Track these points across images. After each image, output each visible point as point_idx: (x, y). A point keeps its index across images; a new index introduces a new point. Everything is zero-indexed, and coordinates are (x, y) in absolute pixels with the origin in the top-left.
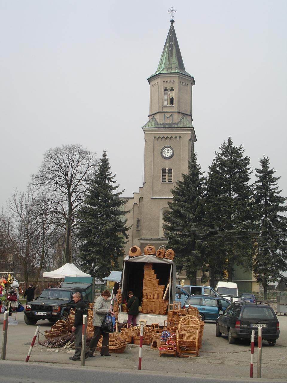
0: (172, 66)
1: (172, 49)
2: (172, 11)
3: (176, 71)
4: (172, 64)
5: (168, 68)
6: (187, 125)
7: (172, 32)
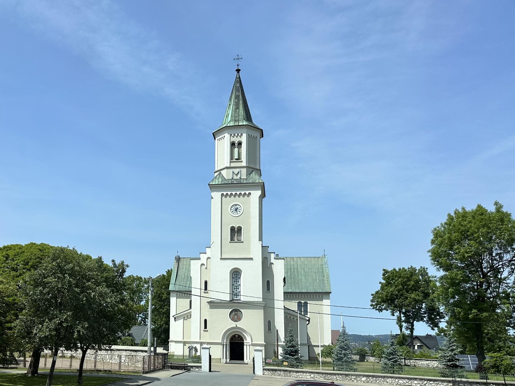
1: (239, 100)
3: (244, 124)
4: (239, 116)
5: (235, 121)
6: (257, 181)
7: (239, 81)
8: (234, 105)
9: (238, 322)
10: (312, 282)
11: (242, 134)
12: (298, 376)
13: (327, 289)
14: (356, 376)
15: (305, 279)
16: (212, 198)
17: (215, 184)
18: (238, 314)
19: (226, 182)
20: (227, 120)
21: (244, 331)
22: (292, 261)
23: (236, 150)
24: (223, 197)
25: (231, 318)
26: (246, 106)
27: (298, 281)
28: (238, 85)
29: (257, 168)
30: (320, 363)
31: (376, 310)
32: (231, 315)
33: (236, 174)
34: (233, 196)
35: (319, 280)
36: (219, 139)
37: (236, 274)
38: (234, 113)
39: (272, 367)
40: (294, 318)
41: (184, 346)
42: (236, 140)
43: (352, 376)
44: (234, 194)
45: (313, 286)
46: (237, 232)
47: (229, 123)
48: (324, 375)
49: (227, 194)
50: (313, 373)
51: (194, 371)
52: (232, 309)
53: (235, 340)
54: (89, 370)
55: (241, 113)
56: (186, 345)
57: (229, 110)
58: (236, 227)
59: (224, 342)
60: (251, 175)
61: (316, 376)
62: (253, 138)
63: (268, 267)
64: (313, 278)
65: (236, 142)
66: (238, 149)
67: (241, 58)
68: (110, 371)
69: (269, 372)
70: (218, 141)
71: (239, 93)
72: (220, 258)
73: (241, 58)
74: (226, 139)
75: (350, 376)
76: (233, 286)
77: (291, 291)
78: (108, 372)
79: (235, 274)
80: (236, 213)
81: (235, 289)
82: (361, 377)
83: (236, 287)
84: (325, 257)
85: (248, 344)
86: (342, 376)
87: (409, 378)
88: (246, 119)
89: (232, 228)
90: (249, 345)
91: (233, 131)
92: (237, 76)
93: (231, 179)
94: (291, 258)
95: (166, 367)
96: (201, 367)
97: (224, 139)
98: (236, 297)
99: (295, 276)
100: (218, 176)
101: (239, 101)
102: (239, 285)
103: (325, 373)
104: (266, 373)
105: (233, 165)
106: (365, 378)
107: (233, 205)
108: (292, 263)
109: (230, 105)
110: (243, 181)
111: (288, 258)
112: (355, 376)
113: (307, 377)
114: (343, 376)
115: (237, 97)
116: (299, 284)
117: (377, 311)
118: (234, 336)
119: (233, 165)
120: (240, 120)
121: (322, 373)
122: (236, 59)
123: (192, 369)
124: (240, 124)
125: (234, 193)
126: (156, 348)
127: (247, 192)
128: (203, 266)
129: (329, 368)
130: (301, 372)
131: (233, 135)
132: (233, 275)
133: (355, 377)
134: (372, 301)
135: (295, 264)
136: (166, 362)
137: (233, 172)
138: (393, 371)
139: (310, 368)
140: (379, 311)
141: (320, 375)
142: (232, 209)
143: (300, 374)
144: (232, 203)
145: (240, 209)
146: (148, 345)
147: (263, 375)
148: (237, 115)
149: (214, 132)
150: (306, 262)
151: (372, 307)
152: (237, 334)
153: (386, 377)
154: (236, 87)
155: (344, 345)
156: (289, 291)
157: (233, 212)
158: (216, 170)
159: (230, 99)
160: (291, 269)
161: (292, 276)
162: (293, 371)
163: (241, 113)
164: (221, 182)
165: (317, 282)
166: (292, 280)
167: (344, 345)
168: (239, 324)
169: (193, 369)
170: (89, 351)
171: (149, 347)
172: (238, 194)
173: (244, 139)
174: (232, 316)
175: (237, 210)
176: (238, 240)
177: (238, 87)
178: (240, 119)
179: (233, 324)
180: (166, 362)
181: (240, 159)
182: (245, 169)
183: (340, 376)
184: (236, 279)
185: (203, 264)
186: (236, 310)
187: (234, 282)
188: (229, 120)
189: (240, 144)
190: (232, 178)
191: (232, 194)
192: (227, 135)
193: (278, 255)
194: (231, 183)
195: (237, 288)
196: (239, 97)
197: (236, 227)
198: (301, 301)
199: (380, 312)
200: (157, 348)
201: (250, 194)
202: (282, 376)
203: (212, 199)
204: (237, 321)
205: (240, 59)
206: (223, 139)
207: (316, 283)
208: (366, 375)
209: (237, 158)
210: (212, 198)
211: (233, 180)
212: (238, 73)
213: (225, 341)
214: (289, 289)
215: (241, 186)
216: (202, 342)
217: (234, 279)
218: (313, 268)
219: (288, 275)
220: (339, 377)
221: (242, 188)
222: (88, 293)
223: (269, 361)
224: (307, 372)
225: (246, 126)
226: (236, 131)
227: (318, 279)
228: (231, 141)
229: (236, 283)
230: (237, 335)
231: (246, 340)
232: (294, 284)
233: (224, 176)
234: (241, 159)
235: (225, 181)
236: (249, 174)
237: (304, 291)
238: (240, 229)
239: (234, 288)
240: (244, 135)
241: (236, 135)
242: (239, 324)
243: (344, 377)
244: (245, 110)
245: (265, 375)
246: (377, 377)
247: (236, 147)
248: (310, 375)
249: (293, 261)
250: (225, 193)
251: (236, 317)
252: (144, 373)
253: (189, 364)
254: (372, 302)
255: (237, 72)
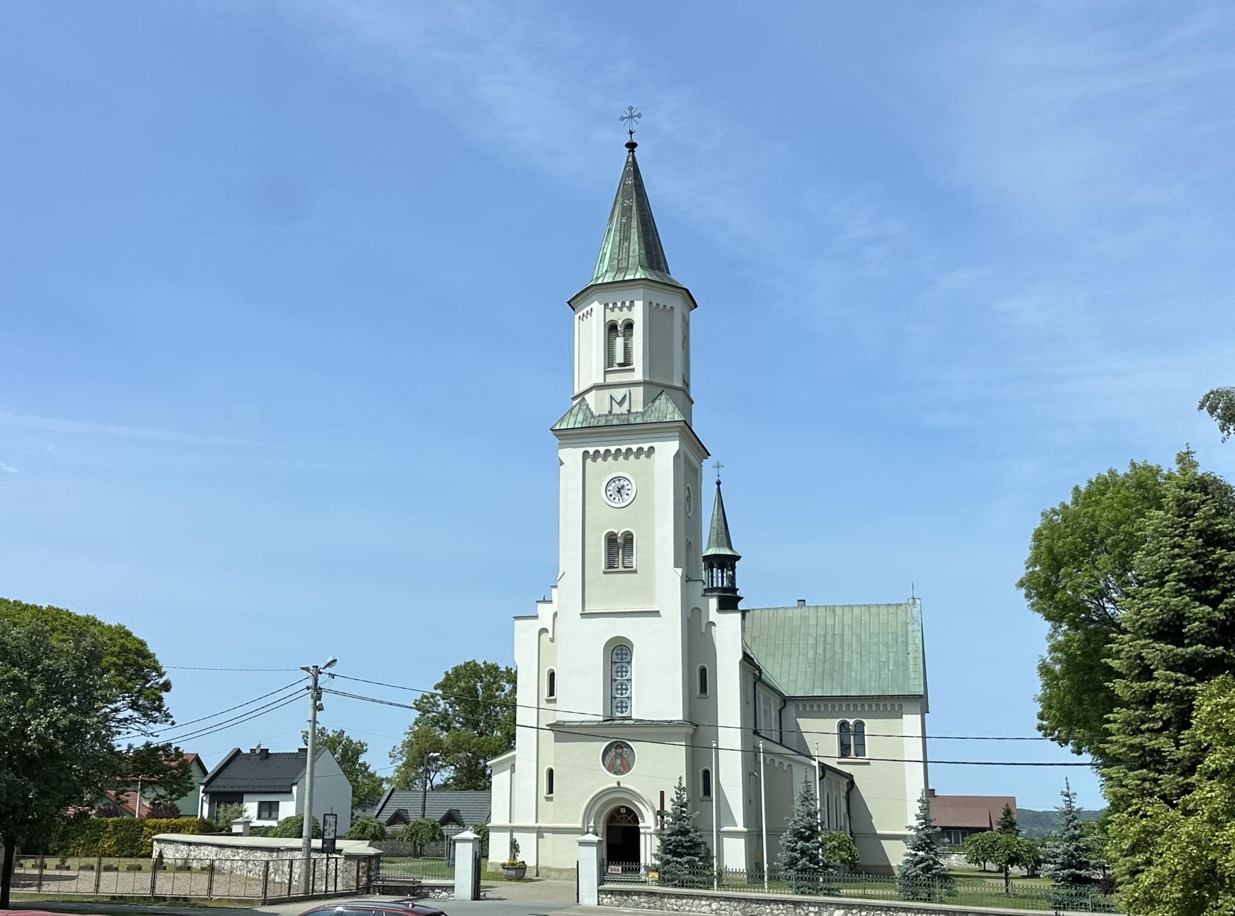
0: (630, 262)
1: (630, 218)
2: (631, 117)
3: (638, 276)
4: (629, 257)
5: (619, 270)
6: (668, 416)
7: (634, 170)
8: (619, 233)
9: (617, 775)
10: (878, 669)
11: (632, 302)
12: (680, 907)
13: (912, 687)
14: (819, 907)
15: (861, 661)
16: (562, 464)
17: (565, 428)
18: (623, 754)
19: (594, 422)
20: (601, 269)
21: (639, 797)
22: (830, 616)
23: (619, 342)
24: (589, 461)
25: (607, 765)
26: (648, 231)
27: (842, 666)
28: (631, 180)
29: (676, 384)
30: (764, 875)
31: (1052, 740)
32: (607, 757)
33: (618, 402)
34: (611, 457)
35: (896, 664)
36: (581, 317)
37: (622, 652)
38: (616, 250)
39: (436, 880)
40: (791, 766)
41: (540, 839)
42: (619, 317)
43: (808, 906)
44: (613, 452)
45: (877, 679)
46: (622, 545)
47: (601, 276)
48: (742, 905)
49: (597, 452)
50: (716, 899)
51: (436, 897)
52: (609, 742)
53: (620, 822)
54: (137, 897)
55: (634, 251)
56: (543, 837)
57: (607, 243)
58: (619, 535)
59: (588, 827)
60: (657, 402)
61: (723, 908)
62: (662, 310)
63: (703, 634)
64: (881, 660)
65: (620, 322)
66: (625, 340)
67: (639, 116)
68: (185, 899)
69: (613, 899)
70: (581, 320)
71: (632, 202)
72: (581, 614)
73: (639, 116)
74: (593, 319)
75: (804, 905)
76: (614, 684)
77: (821, 695)
78: (181, 901)
79: (619, 652)
80: (619, 500)
81: (619, 691)
82: (832, 909)
83: (622, 687)
84: (914, 603)
85: (648, 831)
86: (785, 907)
87: (949, 911)
88: (646, 265)
89: (611, 535)
90: (651, 834)
91: (610, 296)
92: (627, 159)
93: (606, 415)
94: (828, 609)
95: (372, 890)
96: (452, 887)
97: (590, 314)
98: (622, 712)
99: (834, 653)
100: (578, 407)
101: (631, 221)
102: (628, 680)
103: (746, 900)
104: (605, 901)
105: (612, 379)
106: (842, 911)
107: (613, 480)
108: (830, 621)
109: (609, 230)
110: (635, 419)
111: (819, 609)
112: (818, 906)
113: (703, 909)
114: (788, 906)
115: (626, 211)
116: (842, 675)
117: (1056, 743)
118: (617, 811)
119: (612, 379)
120: (631, 269)
121: (738, 898)
122: (626, 118)
123: (432, 895)
124: (627, 278)
125: (613, 449)
126: (335, 842)
127: (646, 447)
128: (544, 635)
129: (852, 891)
130: (688, 898)
131: (611, 305)
132: (614, 656)
133: (817, 909)
134: (1041, 717)
135: (836, 624)
136: (371, 876)
137: (611, 396)
138: (929, 896)
139: (786, 892)
140: (1060, 744)
141: (732, 904)
142: (610, 488)
143: (684, 901)
144: (610, 474)
145: (628, 487)
146: (304, 835)
147: (598, 905)
148: (624, 255)
149: (571, 300)
150: (865, 618)
151: (1040, 734)
152: (623, 807)
153: (893, 909)
154: (625, 187)
155: (805, 827)
156: (815, 695)
157: (611, 495)
158: (576, 392)
159: (611, 218)
160: (825, 636)
161: (828, 656)
162: (670, 895)
163: (634, 251)
164: (582, 423)
165: (890, 668)
166: (827, 665)
167: (805, 827)
168: (627, 780)
169: (434, 892)
170: (242, 852)
171: (306, 839)
172: (624, 451)
173: (637, 314)
174: (607, 762)
175: (622, 491)
176: (625, 567)
177: (629, 186)
178: (632, 264)
179: (611, 780)
180: (371, 876)
181: (629, 365)
182: (641, 389)
183: (781, 905)
184: (621, 664)
185: (543, 630)
186: (619, 743)
187: (617, 672)
188: (605, 269)
189: (629, 326)
190: (610, 412)
191: (608, 451)
192: (597, 307)
193: (804, 601)
194: (604, 424)
195: (624, 687)
196: (631, 211)
197: (619, 535)
198: (848, 720)
199: (1062, 746)
200: (337, 841)
201: (652, 449)
202: (643, 907)
203: (561, 465)
204: (622, 773)
205: (635, 116)
206: (589, 315)
207: (886, 671)
208: (845, 904)
209: (622, 361)
210: (562, 464)
211: (610, 417)
212: (631, 153)
213: (592, 824)
214: (815, 690)
215: (609, 432)
216: (540, 827)
217: (615, 667)
218: (883, 634)
219: (818, 652)
220: (777, 910)
221: (580, 441)
222: (1205, 719)
223: (615, 870)
224: (702, 896)
225: (643, 282)
226: (618, 296)
227: (891, 661)
228: (607, 321)
229: (622, 676)
230: (624, 809)
231: (643, 819)
232: (831, 675)
233: (590, 406)
234: (632, 364)
235: (592, 420)
236: (649, 400)
237: (852, 695)
238: (628, 538)
239: (617, 689)
240: (639, 305)
241: (619, 304)
242: (627, 780)
243: (789, 907)
244: (645, 243)
245: (603, 905)
246: (871, 908)
247: (620, 335)
248: (710, 905)
249: (833, 615)
250: (591, 450)
251: (619, 761)
252: (266, 902)
253: (424, 882)
254: (1042, 719)
255: (628, 150)
